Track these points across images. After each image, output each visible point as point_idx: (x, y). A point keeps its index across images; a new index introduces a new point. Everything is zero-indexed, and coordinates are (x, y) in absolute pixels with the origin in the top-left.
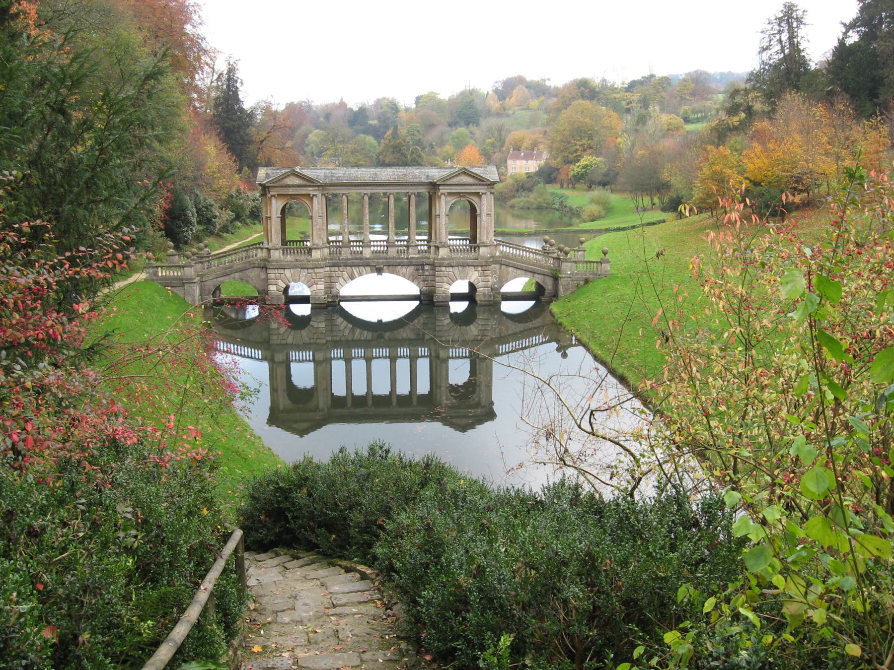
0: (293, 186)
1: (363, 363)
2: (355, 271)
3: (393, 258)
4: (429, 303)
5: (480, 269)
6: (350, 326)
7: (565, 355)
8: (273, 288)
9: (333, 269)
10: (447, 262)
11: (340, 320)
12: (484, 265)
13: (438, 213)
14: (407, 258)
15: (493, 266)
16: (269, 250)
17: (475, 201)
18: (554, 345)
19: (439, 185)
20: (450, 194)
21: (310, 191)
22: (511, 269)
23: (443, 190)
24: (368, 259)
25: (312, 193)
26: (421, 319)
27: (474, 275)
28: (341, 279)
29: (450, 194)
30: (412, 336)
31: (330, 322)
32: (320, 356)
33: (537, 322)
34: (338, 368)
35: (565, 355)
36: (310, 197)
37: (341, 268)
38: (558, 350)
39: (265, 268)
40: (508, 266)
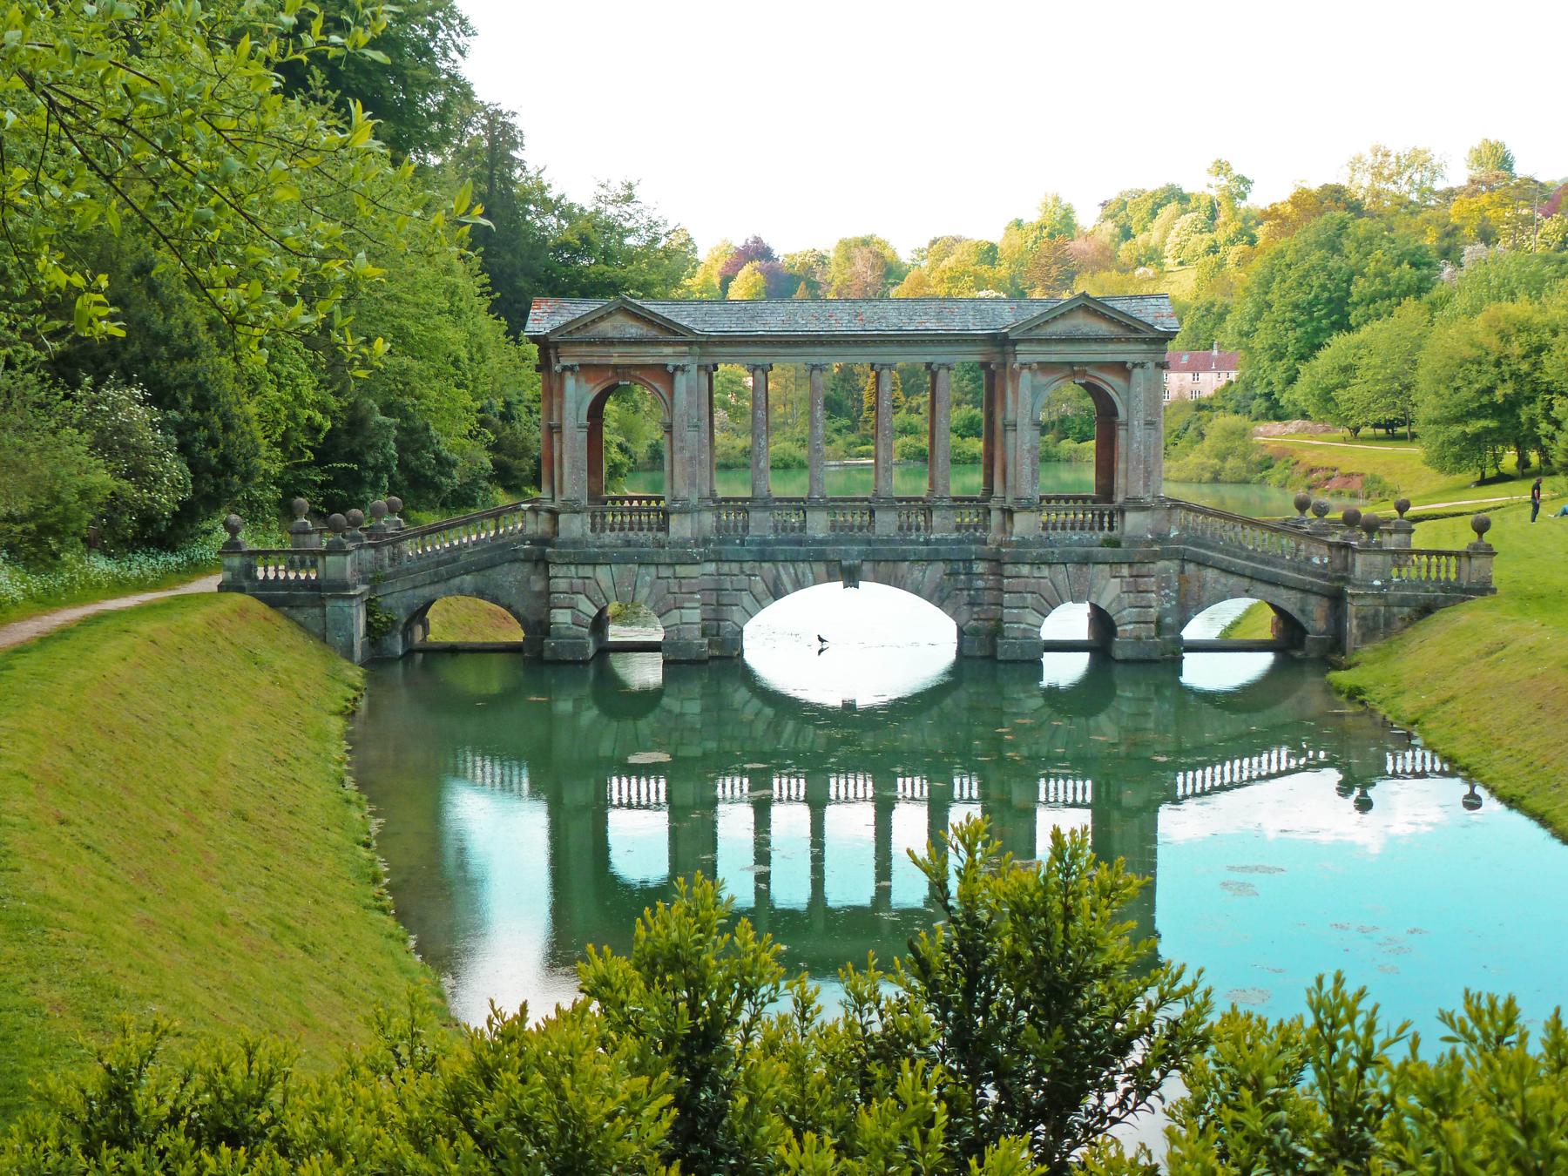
0: (623, 342)
1: (803, 813)
2: (786, 574)
3: (889, 541)
4: (992, 658)
5: (1125, 571)
6: (769, 712)
7: (1364, 805)
8: (562, 617)
9: (725, 568)
10: (1035, 552)
11: (741, 695)
12: (1132, 558)
13: (1010, 417)
14: (927, 542)
15: (1161, 564)
16: (554, 514)
17: (1112, 383)
18: (1333, 776)
19: (1015, 343)
20: (1046, 367)
21: (667, 355)
22: (1210, 574)
23: (1026, 354)
24: (821, 542)
25: (671, 362)
26: (963, 695)
27: (1110, 589)
28: (746, 599)
29: (1046, 367)
30: (936, 742)
31: (717, 707)
32: (688, 792)
33: (1284, 711)
34: (734, 823)
35: (1364, 805)
36: (666, 375)
37: (747, 567)
38: (1344, 789)
39: (541, 562)
40: (1202, 563)
